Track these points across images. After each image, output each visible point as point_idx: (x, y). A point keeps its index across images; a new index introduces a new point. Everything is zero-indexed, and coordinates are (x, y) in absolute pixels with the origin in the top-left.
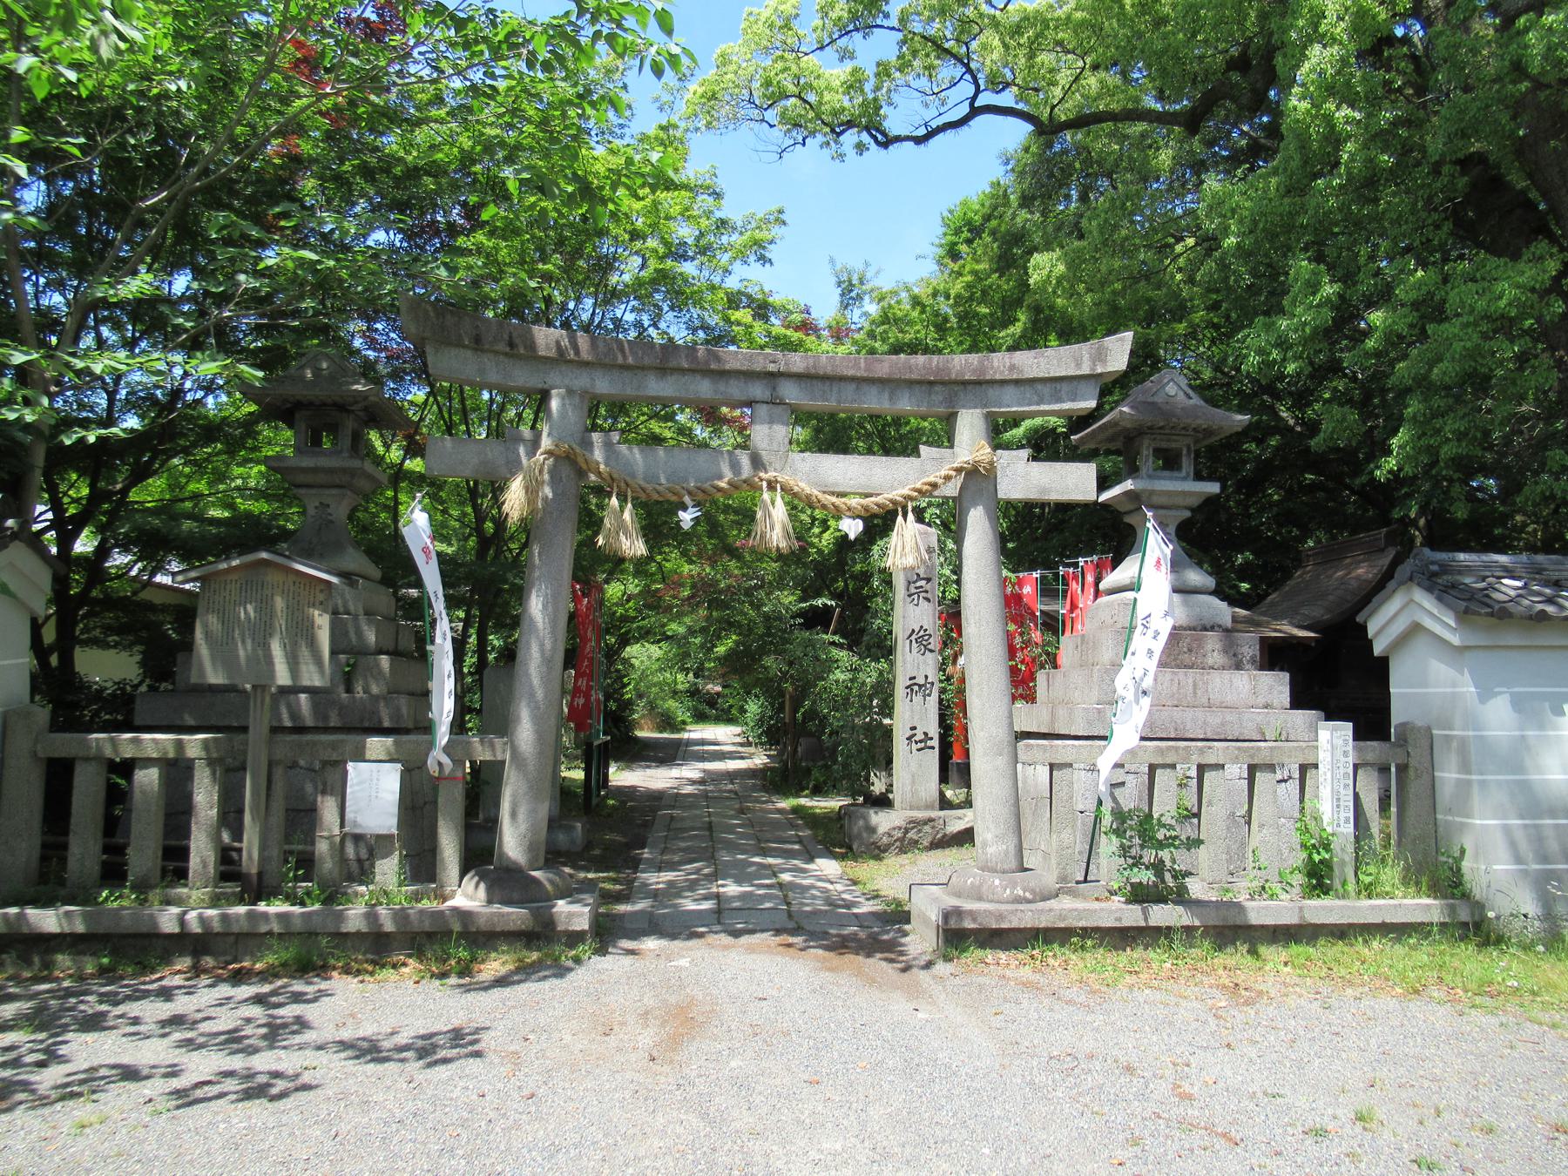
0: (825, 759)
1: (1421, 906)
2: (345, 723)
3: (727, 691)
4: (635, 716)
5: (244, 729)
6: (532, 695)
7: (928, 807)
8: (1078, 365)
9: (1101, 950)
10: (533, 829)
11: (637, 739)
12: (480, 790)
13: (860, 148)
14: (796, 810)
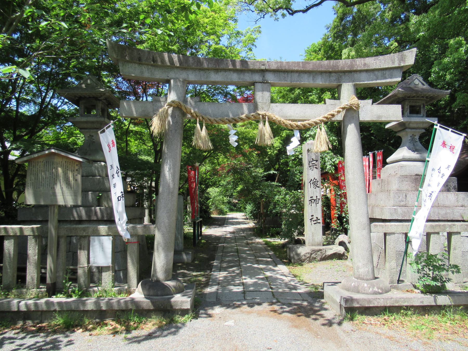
0: (277, 227)
3: (239, 202)
4: (211, 210)
7: (319, 245)
8: (393, 63)
9: (415, 316)
10: (167, 263)
12: (146, 246)
13: (284, 15)
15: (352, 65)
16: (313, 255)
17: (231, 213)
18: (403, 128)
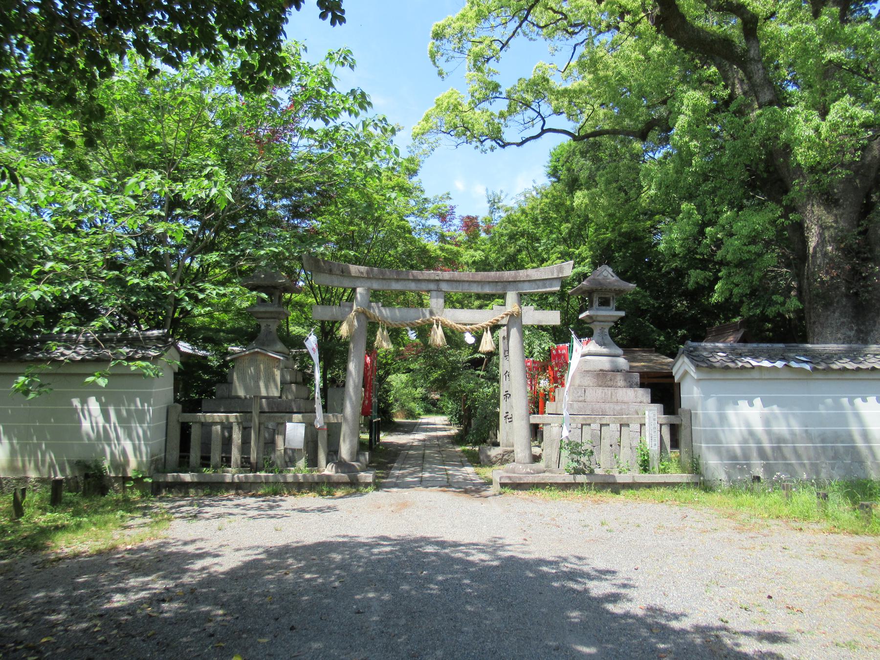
0: (477, 428)
1: (685, 477)
2: (280, 411)
4: (394, 411)
5: (251, 412)
6: (351, 399)
8: (553, 274)
10: (352, 447)
11: (394, 423)
12: (333, 432)
13: (492, 149)
14: (463, 451)
15: (516, 276)
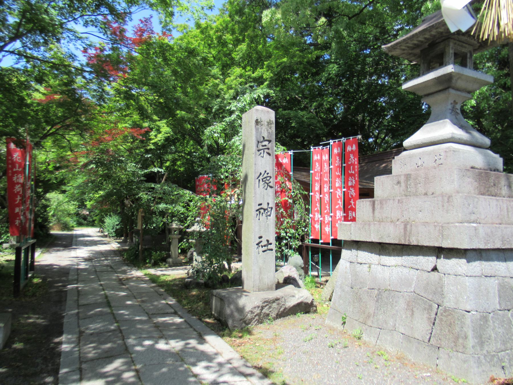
4: (51, 225)
11: (52, 235)
16: (265, 310)
17: (80, 228)
18: (441, 88)
